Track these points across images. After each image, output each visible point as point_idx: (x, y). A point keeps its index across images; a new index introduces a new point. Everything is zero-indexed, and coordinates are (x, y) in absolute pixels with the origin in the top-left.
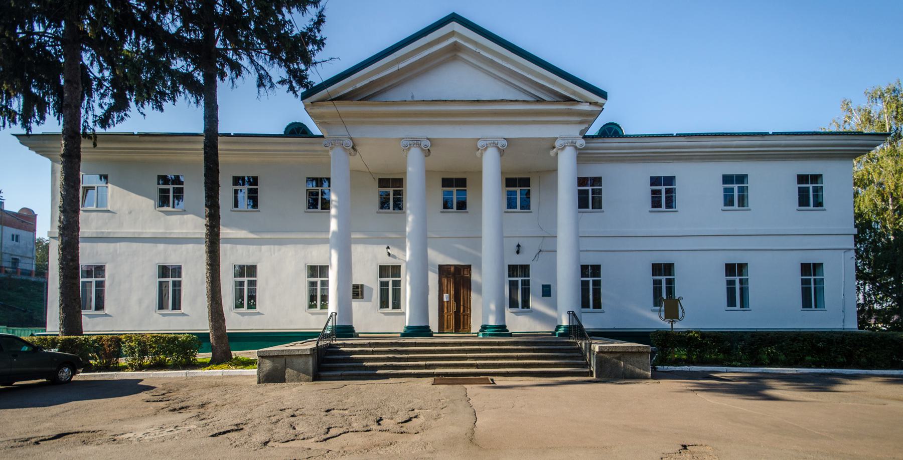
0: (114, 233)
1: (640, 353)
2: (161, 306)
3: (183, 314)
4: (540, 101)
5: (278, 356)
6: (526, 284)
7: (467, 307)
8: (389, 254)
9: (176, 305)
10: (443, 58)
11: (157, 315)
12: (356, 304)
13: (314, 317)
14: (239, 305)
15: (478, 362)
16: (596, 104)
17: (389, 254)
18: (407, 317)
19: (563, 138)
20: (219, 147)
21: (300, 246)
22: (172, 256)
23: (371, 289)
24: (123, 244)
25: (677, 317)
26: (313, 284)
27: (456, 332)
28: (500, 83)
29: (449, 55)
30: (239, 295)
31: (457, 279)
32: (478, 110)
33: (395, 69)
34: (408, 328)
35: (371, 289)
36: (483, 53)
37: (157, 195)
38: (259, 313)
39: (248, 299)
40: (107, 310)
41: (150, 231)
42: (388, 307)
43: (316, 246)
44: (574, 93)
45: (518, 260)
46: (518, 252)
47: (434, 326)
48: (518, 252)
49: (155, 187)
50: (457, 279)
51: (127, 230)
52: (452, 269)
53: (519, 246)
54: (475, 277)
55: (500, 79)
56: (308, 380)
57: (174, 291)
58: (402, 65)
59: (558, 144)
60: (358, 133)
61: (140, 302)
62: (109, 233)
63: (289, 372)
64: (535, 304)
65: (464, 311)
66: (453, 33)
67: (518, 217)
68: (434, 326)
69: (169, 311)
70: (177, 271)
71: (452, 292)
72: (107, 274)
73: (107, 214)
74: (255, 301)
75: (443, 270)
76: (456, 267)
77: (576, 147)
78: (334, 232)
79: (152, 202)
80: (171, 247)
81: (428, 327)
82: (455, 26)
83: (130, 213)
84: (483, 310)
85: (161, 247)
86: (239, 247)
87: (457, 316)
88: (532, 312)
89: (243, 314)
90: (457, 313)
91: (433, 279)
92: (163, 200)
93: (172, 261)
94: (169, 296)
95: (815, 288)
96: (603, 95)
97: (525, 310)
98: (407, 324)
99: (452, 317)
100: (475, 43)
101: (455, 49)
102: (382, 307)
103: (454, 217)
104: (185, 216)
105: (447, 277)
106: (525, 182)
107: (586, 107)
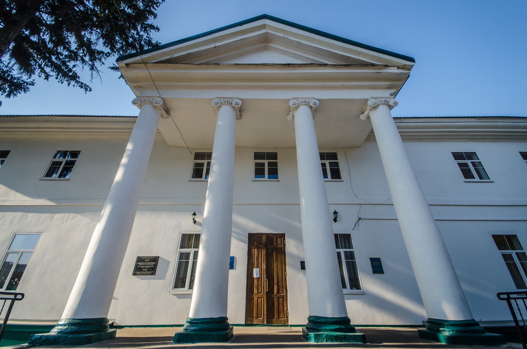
6: (350, 256)
7: (283, 286)
8: (195, 222)
10: (256, 46)
16: (404, 67)
17: (195, 222)
18: (192, 306)
23: (168, 263)
27: (270, 323)
29: (262, 45)
31: (268, 249)
34: (192, 322)
35: (168, 263)
42: (184, 287)
45: (340, 228)
46: (335, 220)
47: (235, 313)
48: (335, 220)
50: (268, 249)
52: (264, 237)
53: (335, 213)
54: (291, 246)
59: (370, 103)
60: (168, 95)
64: (368, 283)
65: (278, 292)
66: (264, 26)
67: (333, 185)
68: (235, 313)
71: (264, 266)
74: (19, 280)
75: (254, 240)
76: (267, 235)
81: (223, 320)
84: (306, 297)
86: (30, 215)
87: (268, 299)
88: (364, 294)
90: (270, 294)
91: (239, 249)
95: (522, 264)
96: (412, 60)
97: (355, 291)
98: (191, 315)
99: (263, 302)
100: (284, 31)
102: (176, 286)
103: (266, 185)
105: (258, 248)
106: (334, 156)
107: (394, 70)
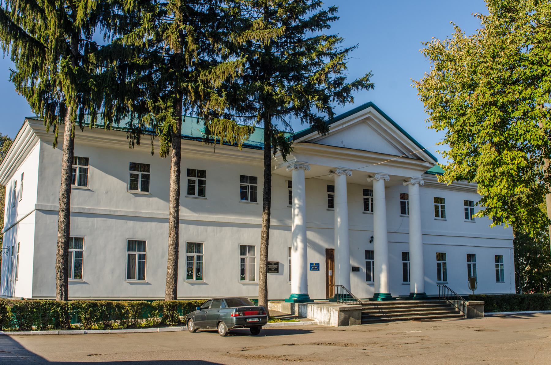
0: (94, 209)
1: (481, 305)
2: (130, 276)
3: (148, 284)
4: (407, 158)
5: (347, 311)
9: (142, 276)
11: (126, 283)
12: (271, 277)
13: (245, 286)
14: (190, 276)
15: (420, 312)
19: (415, 179)
20: (182, 146)
21: (235, 228)
22: (139, 231)
24: (99, 219)
25: (474, 288)
26: (243, 260)
28: (385, 141)
30: (189, 269)
32: (377, 157)
33: (341, 127)
36: (382, 126)
37: (128, 178)
38: (205, 284)
39: (195, 272)
40: (84, 279)
41: (123, 210)
42: (134, 278)
43: (247, 229)
44: (423, 156)
49: (128, 172)
51: (103, 208)
55: (386, 139)
56: (359, 324)
57: (140, 262)
58: (344, 126)
61: (113, 272)
62: (90, 209)
63: (351, 319)
66: (370, 112)
69: (136, 280)
70: (142, 245)
72: (85, 247)
73: (87, 192)
77: (420, 184)
78: (297, 226)
79: (125, 184)
80: (139, 224)
82: (371, 109)
83: (107, 193)
85: (131, 223)
89: (192, 284)
92: (133, 186)
93: (139, 237)
94: (136, 269)
97: (78, 280)
100: (380, 120)
101: (368, 118)
104: (151, 199)
107: (427, 164)
